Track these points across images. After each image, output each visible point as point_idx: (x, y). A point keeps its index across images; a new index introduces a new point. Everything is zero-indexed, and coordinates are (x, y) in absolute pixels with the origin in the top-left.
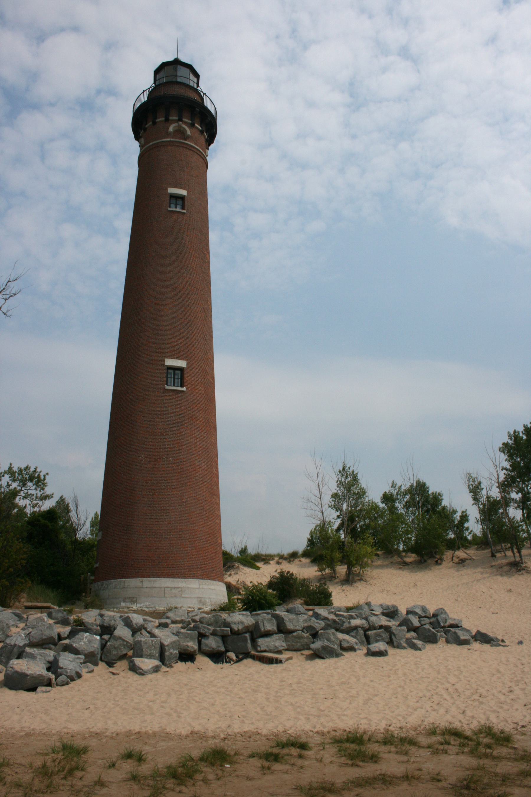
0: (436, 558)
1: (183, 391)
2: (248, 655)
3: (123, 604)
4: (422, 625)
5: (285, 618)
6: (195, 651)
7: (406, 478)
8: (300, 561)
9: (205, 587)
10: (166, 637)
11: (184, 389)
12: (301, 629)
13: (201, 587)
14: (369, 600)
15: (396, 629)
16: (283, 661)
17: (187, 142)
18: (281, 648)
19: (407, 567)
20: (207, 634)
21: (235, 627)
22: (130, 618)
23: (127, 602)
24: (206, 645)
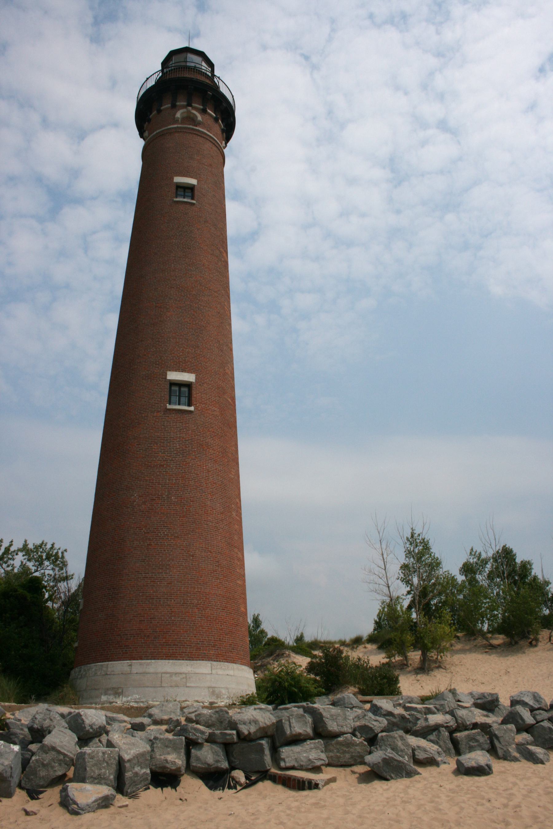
0: (529, 638)
1: (191, 412)
2: (264, 775)
3: (104, 698)
4: (538, 722)
5: (324, 714)
6: (179, 769)
7: (487, 544)
8: (365, 647)
9: (220, 672)
10: (130, 746)
11: (192, 408)
12: (350, 731)
13: (214, 672)
14: (452, 687)
15: (499, 729)
16: (320, 786)
17: (197, 128)
18: (318, 763)
19: (494, 651)
20: (200, 741)
21: (245, 729)
22: (81, 716)
23: (110, 695)
24: (198, 759)
